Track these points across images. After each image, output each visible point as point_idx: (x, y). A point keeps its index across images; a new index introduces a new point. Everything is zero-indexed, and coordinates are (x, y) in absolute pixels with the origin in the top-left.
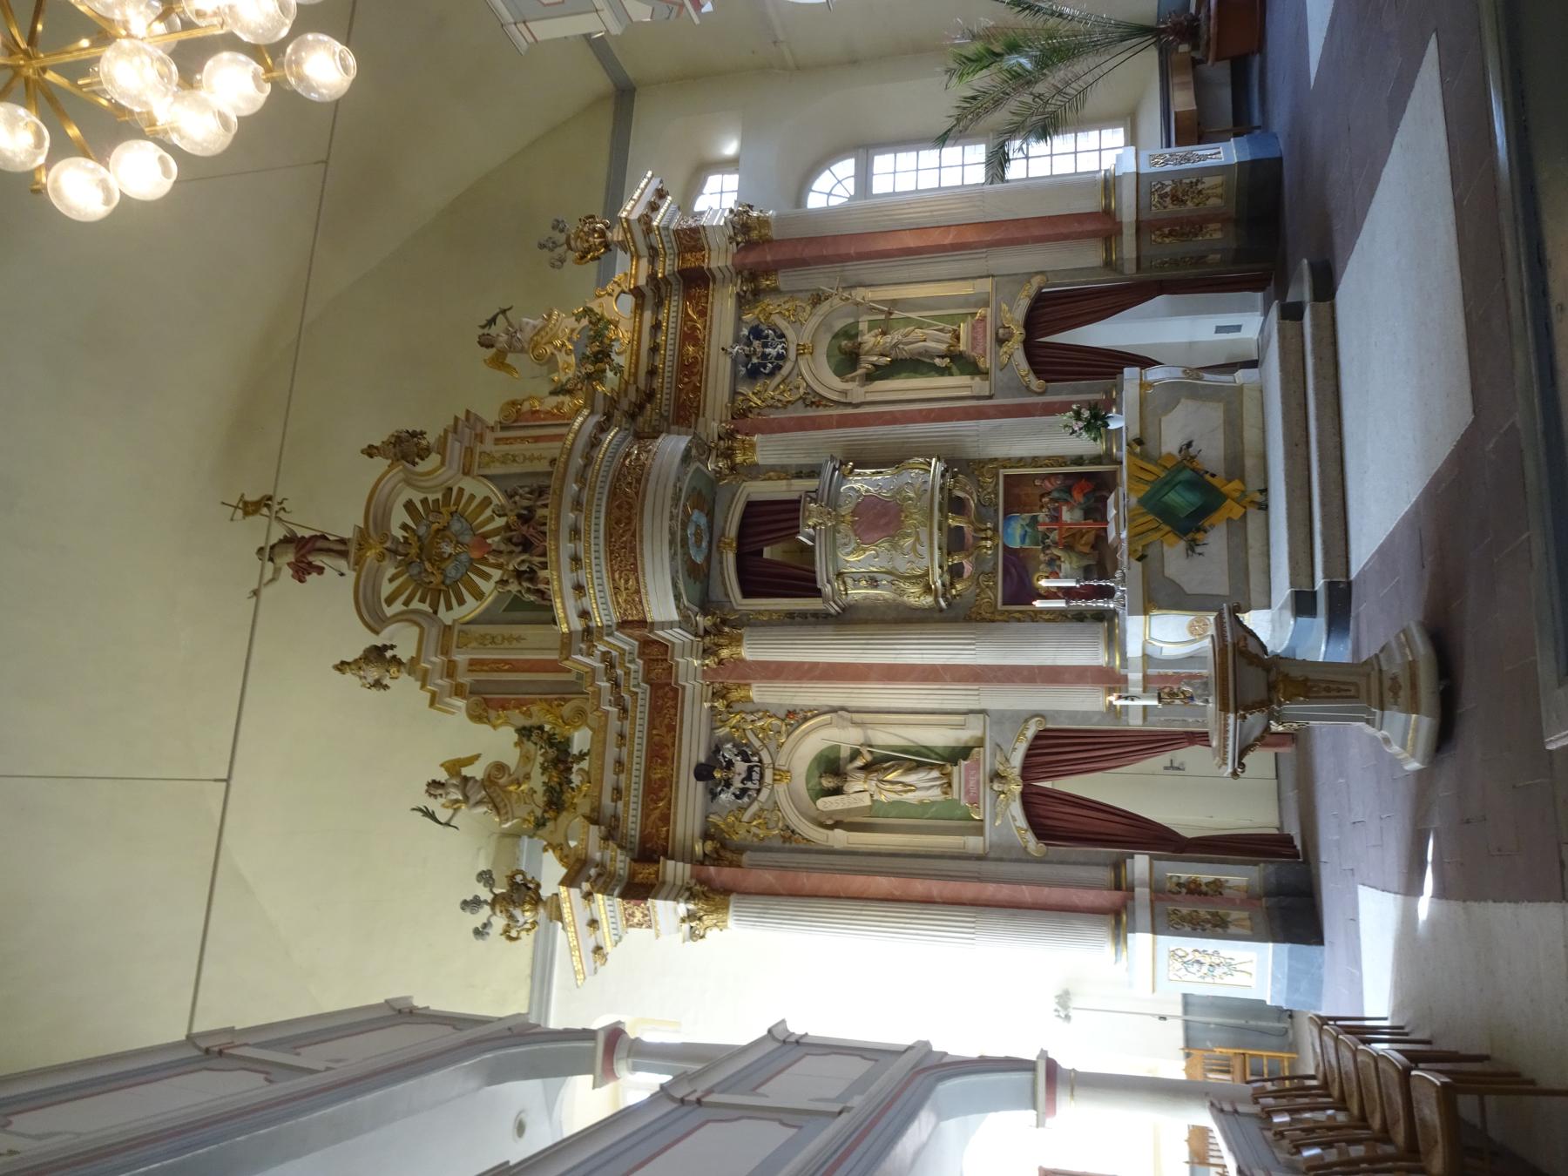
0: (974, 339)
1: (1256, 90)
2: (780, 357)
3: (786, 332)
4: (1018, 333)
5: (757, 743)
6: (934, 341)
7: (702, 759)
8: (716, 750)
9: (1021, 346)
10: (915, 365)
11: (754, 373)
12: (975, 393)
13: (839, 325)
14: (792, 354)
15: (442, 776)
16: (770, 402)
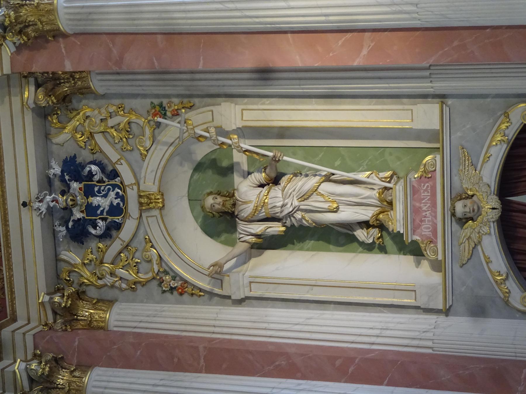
0: (416, 211)
1: (282, 26)
2: (115, 210)
3: (119, 168)
4: (490, 206)
6: (348, 203)
9: (493, 229)
10: (338, 236)
11: (79, 234)
12: (422, 302)
13: (202, 151)
14: (133, 207)
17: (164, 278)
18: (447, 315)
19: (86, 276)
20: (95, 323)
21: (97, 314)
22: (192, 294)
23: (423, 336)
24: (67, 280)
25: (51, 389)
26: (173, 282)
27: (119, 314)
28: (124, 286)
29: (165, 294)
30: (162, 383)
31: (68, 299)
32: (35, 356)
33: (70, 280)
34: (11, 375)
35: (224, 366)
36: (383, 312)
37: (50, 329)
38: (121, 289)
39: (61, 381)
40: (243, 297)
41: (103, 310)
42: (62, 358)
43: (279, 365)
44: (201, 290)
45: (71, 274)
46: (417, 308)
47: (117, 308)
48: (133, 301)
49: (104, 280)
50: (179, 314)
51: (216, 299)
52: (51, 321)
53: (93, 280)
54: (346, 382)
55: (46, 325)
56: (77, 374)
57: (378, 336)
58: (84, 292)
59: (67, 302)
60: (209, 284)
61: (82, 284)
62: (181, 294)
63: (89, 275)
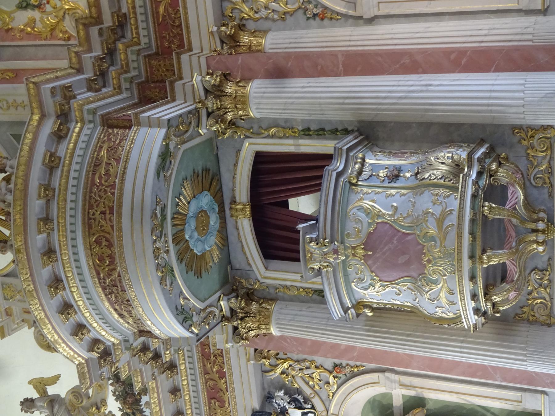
5: (308, 391)
7: (257, 407)
8: (268, 398)
15: (35, 395)
16: (264, 13)
17: (308, 7)
18: (545, 15)
19: (245, 11)
20: (254, 48)
21: (254, 41)
22: (331, 18)
23: (525, 31)
24: (229, 16)
25: (221, 96)
26: (315, 9)
27: (273, 39)
28: (276, 17)
29: (309, 21)
30: (309, 85)
31: (231, 28)
32: (208, 74)
33: (232, 16)
34: (191, 88)
35: (359, 69)
36: (490, 18)
37: (219, 54)
38: (273, 20)
39: (229, 91)
40: (373, 16)
41: (260, 37)
42: (229, 74)
43: (404, 63)
44: (338, 14)
45: (233, 11)
46: (519, 11)
47: (270, 35)
48: (284, 30)
49: (260, 13)
50: (320, 34)
51: (351, 21)
52: (219, 48)
53: (251, 14)
54: (459, 72)
55: (215, 51)
56: (241, 84)
57: (486, 35)
58: (244, 25)
59: (231, 31)
60: (344, 8)
61: (242, 19)
62: (322, 19)
63: (247, 10)
